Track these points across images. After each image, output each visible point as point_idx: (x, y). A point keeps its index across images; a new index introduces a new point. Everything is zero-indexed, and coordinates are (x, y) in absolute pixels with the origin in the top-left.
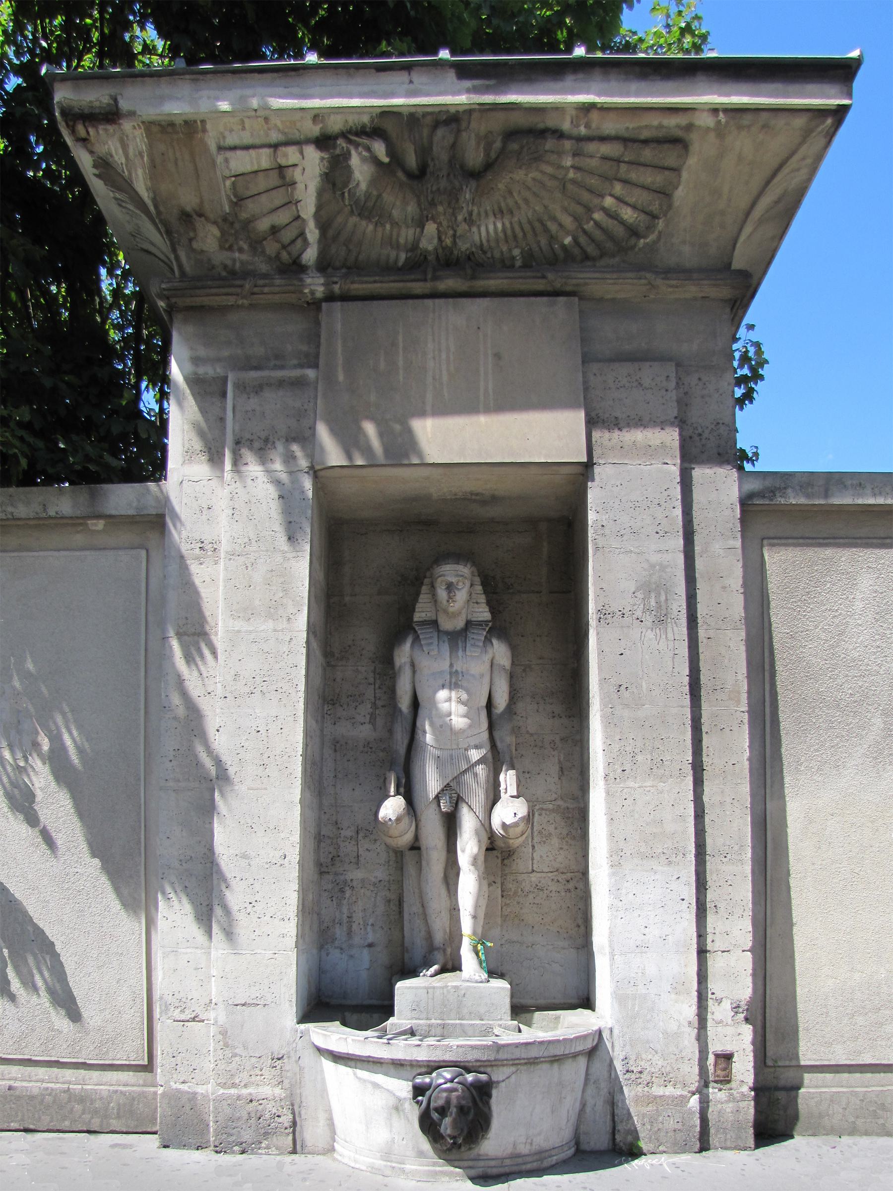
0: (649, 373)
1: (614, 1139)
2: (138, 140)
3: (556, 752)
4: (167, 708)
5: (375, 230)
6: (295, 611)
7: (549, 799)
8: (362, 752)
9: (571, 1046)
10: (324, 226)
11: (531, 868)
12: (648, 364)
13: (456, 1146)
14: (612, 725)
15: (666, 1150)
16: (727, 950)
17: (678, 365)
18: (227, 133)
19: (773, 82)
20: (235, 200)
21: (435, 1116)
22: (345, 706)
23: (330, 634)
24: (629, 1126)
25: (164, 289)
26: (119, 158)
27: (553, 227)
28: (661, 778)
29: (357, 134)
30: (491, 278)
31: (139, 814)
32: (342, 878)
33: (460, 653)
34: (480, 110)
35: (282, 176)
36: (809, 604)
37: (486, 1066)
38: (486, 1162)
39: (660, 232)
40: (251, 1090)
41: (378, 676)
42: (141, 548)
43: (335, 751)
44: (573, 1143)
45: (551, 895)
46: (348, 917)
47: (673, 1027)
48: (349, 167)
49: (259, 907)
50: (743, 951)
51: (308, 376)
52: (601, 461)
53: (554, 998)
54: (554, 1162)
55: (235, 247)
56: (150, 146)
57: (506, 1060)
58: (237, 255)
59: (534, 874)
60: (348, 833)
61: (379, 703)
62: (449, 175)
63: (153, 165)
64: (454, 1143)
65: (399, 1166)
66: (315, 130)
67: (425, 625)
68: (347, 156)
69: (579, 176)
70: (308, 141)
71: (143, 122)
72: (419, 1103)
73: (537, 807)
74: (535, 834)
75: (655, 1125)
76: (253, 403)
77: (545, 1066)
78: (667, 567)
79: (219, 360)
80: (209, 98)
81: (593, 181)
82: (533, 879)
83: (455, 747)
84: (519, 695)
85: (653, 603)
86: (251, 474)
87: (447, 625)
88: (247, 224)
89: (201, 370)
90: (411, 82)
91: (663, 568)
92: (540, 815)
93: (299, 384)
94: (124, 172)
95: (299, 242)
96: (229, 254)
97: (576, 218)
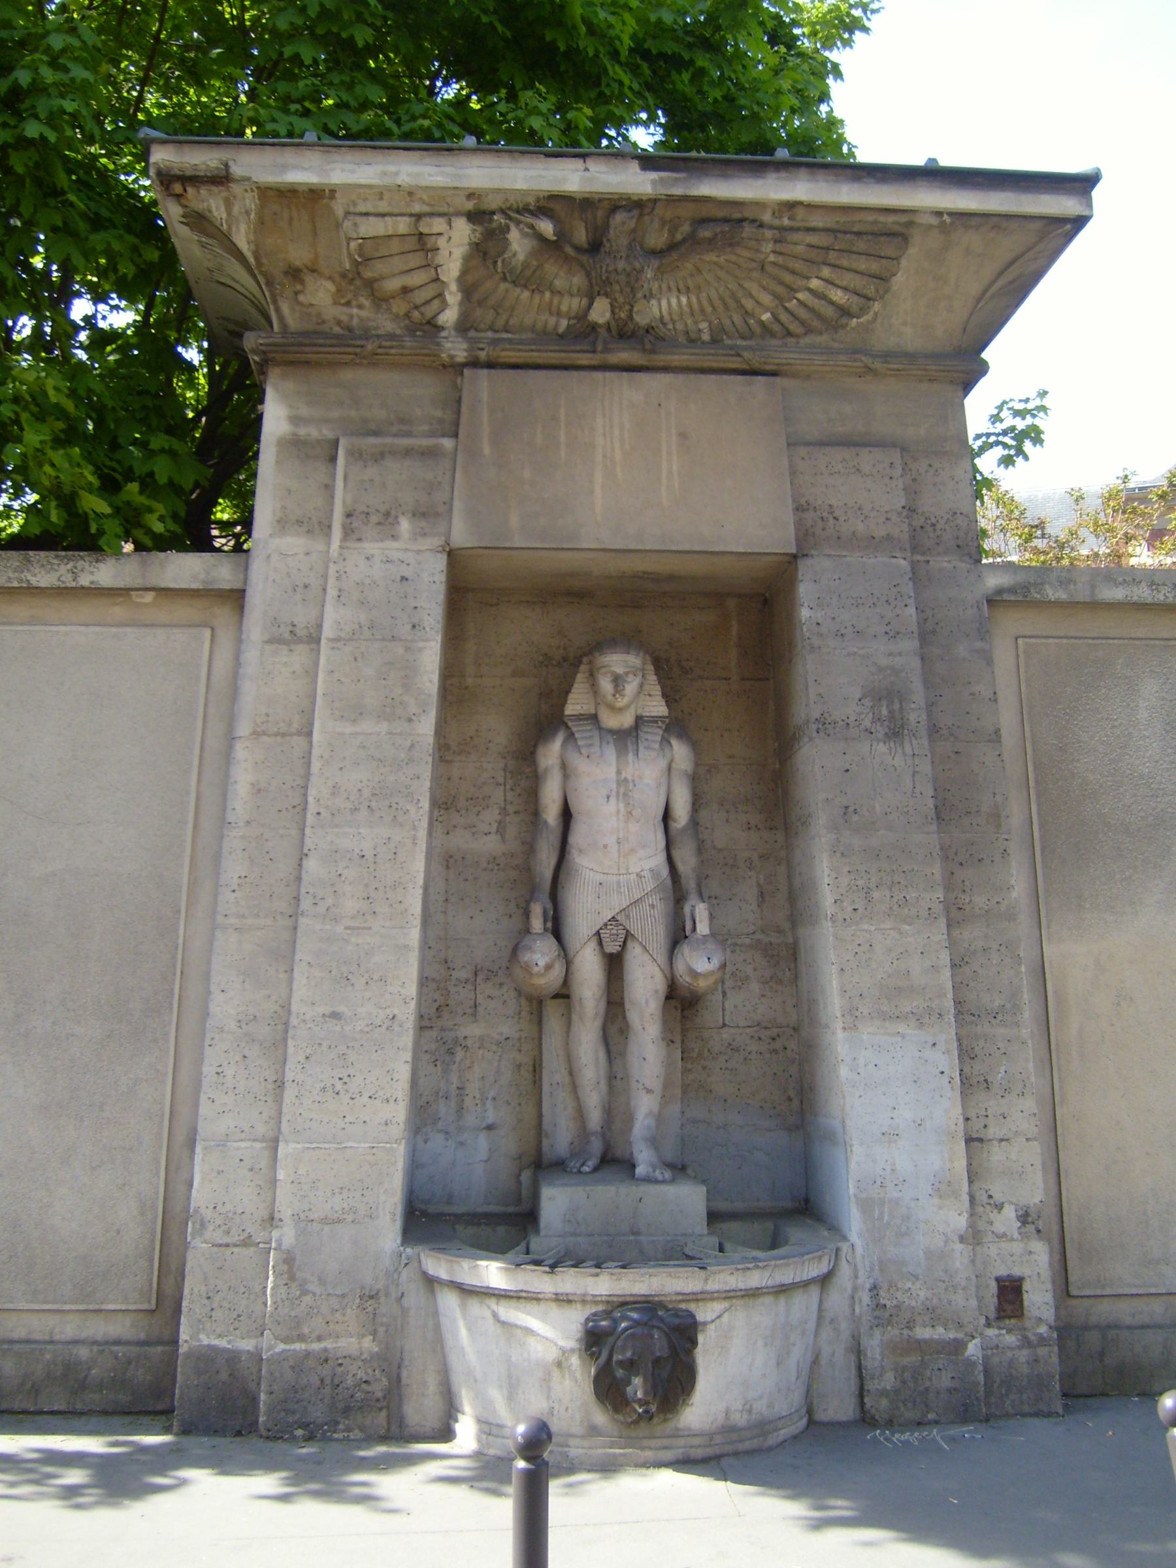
0: (867, 459)
1: (862, 1404)
4: (233, 825)
8: (485, 870)
10: (468, 290)
12: (868, 449)
13: (648, 1416)
14: (838, 854)
15: (937, 1418)
16: (1006, 1137)
17: (903, 450)
19: (1002, 191)
21: (620, 1373)
22: (463, 812)
23: (446, 722)
24: (883, 1384)
25: (261, 344)
27: (749, 304)
29: (518, 212)
30: (675, 354)
31: (174, 957)
32: (451, 1034)
33: (631, 757)
34: (666, 200)
37: (689, 1301)
38: (689, 1439)
40: (328, 1344)
41: (509, 776)
42: (205, 626)
43: (448, 867)
44: (804, 1410)
45: (750, 1057)
46: (458, 1088)
50: (1027, 1140)
51: (443, 445)
52: (813, 552)
53: (758, 1200)
54: (781, 1438)
55: (354, 303)
57: (718, 1292)
58: (355, 311)
59: (726, 1030)
60: (463, 975)
61: (511, 809)
62: (628, 256)
63: (261, 221)
64: (646, 1412)
66: (470, 205)
67: (581, 720)
69: (780, 260)
70: (458, 214)
71: (258, 188)
75: (920, 1382)
76: (371, 471)
77: (768, 1300)
79: (327, 421)
80: (343, 170)
81: (798, 265)
82: (725, 1036)
83: (623, 871)
84: (701, 801)
85: (884, 712)
87: (611, 721)
88: (370, 284)
89: (302, 431)
90: (587, 169)
93: (431, 454)
94: (222, 225)
95: (436, 304)
96: (345, 309)
97: (776, 296)
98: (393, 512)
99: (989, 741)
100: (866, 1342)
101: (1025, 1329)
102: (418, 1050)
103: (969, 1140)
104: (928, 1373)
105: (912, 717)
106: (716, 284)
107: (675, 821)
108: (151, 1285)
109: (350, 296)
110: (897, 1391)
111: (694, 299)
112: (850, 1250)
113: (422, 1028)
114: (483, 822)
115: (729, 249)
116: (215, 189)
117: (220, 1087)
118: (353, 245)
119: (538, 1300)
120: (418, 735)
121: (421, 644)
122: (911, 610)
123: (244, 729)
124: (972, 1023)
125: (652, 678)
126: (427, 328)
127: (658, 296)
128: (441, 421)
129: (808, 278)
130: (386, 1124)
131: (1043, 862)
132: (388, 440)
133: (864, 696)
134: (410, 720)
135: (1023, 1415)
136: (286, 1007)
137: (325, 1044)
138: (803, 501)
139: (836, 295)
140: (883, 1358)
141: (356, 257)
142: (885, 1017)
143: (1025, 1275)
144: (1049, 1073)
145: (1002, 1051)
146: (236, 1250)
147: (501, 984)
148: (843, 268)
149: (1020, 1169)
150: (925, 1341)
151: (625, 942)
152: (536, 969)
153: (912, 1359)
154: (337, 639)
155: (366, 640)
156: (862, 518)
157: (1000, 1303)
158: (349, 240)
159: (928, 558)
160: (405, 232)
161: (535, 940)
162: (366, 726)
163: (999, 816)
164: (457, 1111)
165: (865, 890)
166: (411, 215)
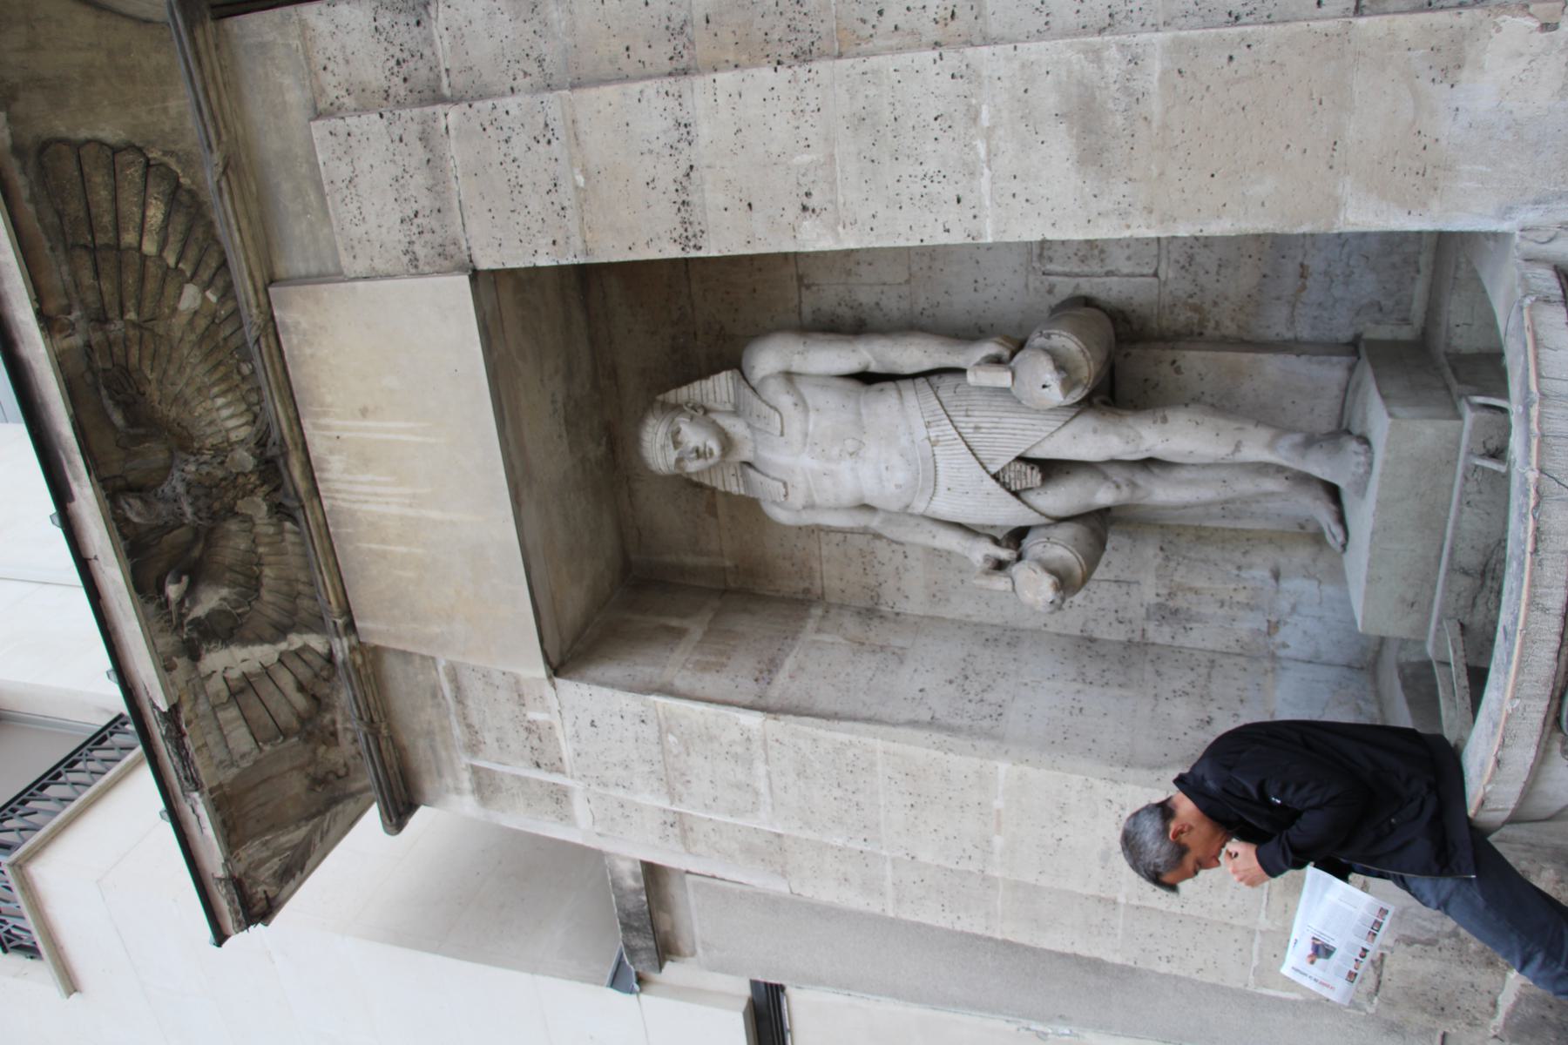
2: (250, 852)
5: (269, 564)
10: (281, 632)
18: (216, 761)
20: (282, 738)
26: (275, 864)
35: (242, 691)
39: (165, 153)
48: (208, 616)
55: (331, 728)
56: (253, 837)
63: (272, 828)
66: (182, 663)
68: (197, 623)
69: (130, 304)
71: (231, 853)
73: (1037, 265)
74: (1086, 269)
76: (489, 737)
81: (130, 280)
82: (1171, 275)
92: (1051, 260)
95: (307, 656)
98: (525, 724)
106: (188, 370)
112: (1531, 235)
114: (891, 559)
139: (155, 216)
160: (237, 708)
164: (1252, 610)
165: (927, 182)
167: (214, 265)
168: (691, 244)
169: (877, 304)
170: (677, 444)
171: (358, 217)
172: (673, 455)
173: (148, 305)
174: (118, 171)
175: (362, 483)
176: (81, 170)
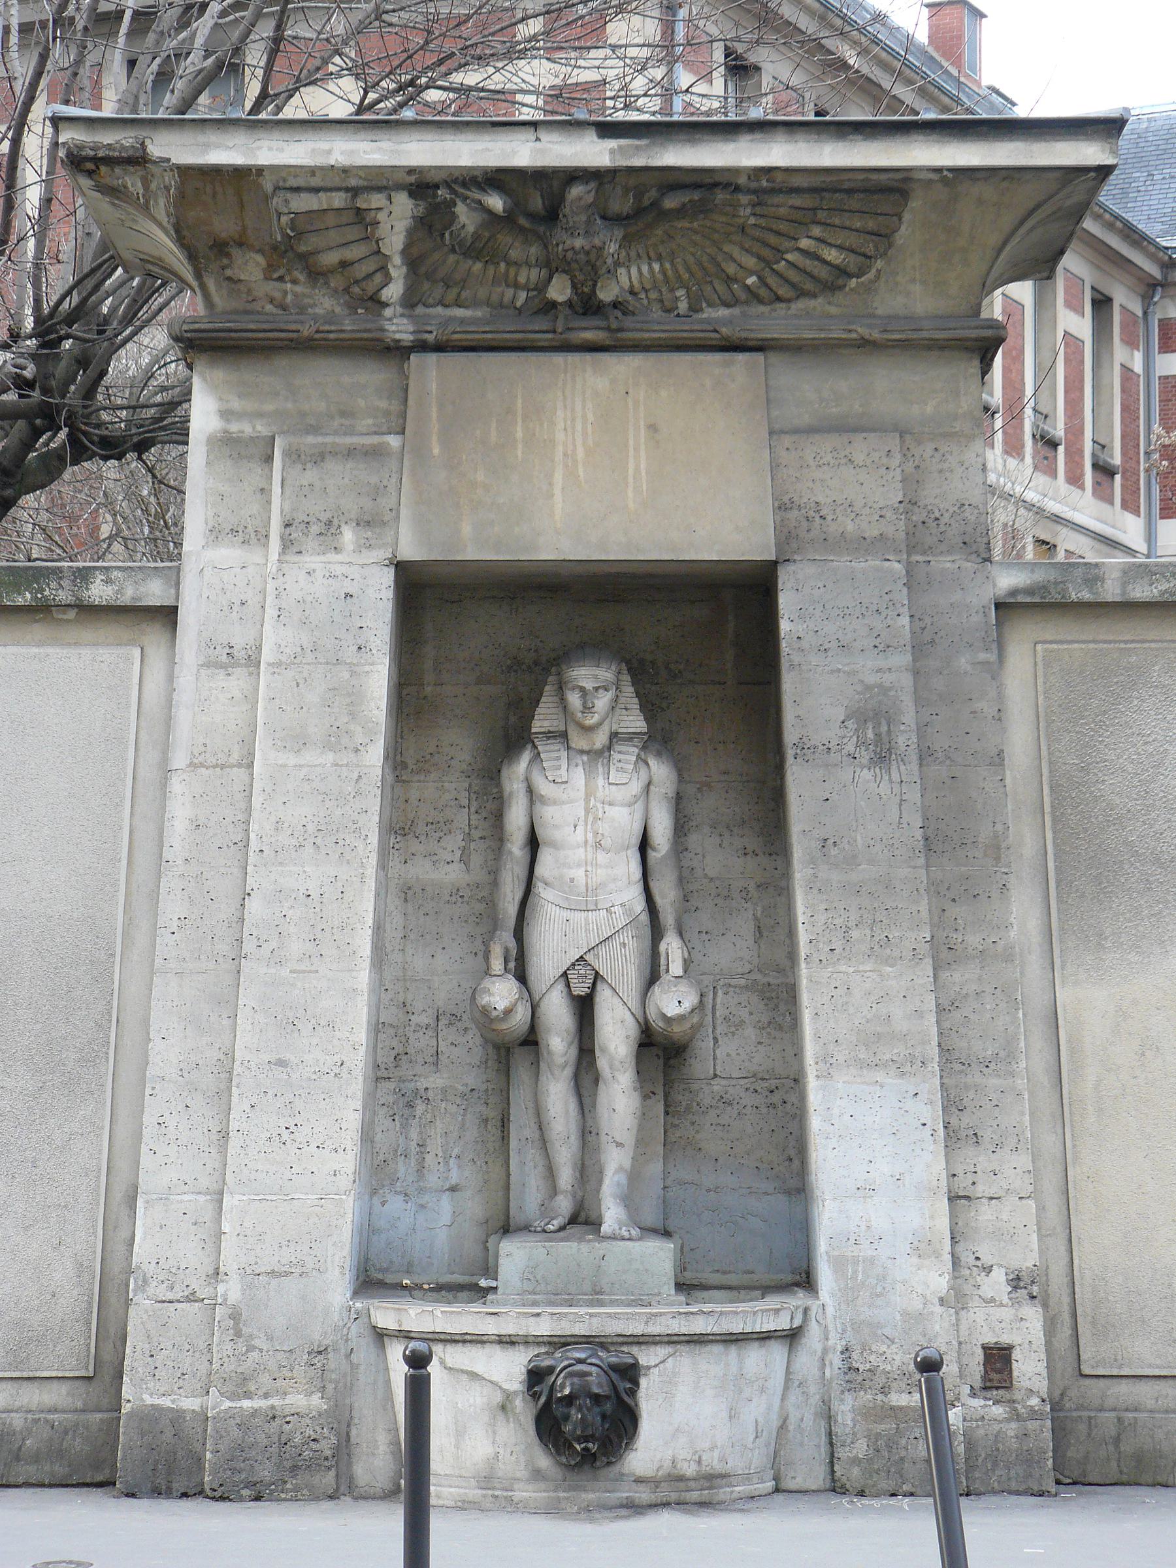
0: (861, 448)
3: (749, 904)
6: (367, 740)
7: (740, 970)
9: (754, 1322)
10: (413, 262)
11: (712, 1072)
14: (815, 891)
15: (913, 1490)
16: (996, 1196)
22: (423, 838)
23: (402, 737)
25: (186, 331)
27: (731, 269)
28: (888, 961)
29: (464, 184)
32: (412, 1085)
36: (1107, 726)
37: (631, 1343)
39: (879, 271)
40: (274, 1401)
41: (473, 796)
43: (406, 900)
45: (744, 1111)
47: (916, 1304)
49: (301, 1135)
51: (389, 444)
52: (796, 557)
58: (289, 285)
60: (423, 1019)
61: (476, 834)
63: (182, 195)
65: (505, 1494)
69: (762, 222)
70: (399, 187)
72: (535, 1396)
73: (721, 983)
74: (719, 1022)
76: (311, 475)
78: (890, 689)
79: (260, 415)
80: (270, 149)
81: (783, 227)
82: (715, 1088)
84: (691, 823)
85: (870, 734)
86: (307, 566)
89: (234, 427)
90: (538, 139)
91: (884, 690)
92: (726, 993)
93: (376, 453)
95: (378, 278)
96: (278, 285)
97: (760, 258)
98: (336, 522)
99: (990, 764)
100: (835, 1405)
101: (1014, 1401)
102: (371, 1103)
103: (954, 1198)
104: (903, 1442)
105: (901, 740)
106: (692, 250)
107: (654, 849)
108: (88, 1350)
109: (281, 272)
110: (870, 1461)
111: (668, 266)
112: (820, 1311)
113: (378, 1079)
115: (702, 216)
116: (131, 169)
117: (162, 1139)
118: (284, 219)
119: (483, 1342)
120: (366, 766)
121: (367, 668)
122: (905, 620)
123: (179, 760)
124: (961, 1072)
125: (629, 689)
126: (369, 304)
127: (627, 264)
128: (387, 413)
129: (796, 239)
130: (335, 1175)
131: (1058, 897)
132: (329, 439)
133: (848, 717)
134: (357, 750)
135: (1010, 1493)
136: (230, 1054)
137: (270, 1093)
138: (786, 499)
140: (855, 1425)
141: (289, 231)
142: (863, 1065)
143: (1015, 1343)
144: (1062, 1131)
145: (995, 1102)
146: (179, 1306)
147: (466, 1029)
148: (836, 226)
149: (1012, 1231)
150: (901, 1408)
151: (594, 984)
152: (495, 1013)
153: (887, 1426)
154: (279, 664)
155: (309, 664)
156: (853, 515)
157: (986, 1372)
158: (279, 215)
159: (929, 559)
161: (494, 983)
162: (310, 757)
163: (999, 848)
166: (347, 190)
167: (780, 292)
168: (798, 751)
169: (687, 849)
170: (597, 689)
171: (821, 462)
172: (589, 685)
173: (758, 233)
174: (873, 237)
175: (584, 408)
176: (881, 214)
